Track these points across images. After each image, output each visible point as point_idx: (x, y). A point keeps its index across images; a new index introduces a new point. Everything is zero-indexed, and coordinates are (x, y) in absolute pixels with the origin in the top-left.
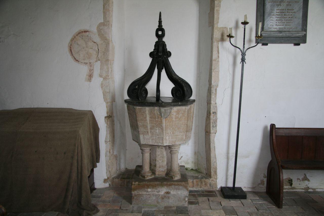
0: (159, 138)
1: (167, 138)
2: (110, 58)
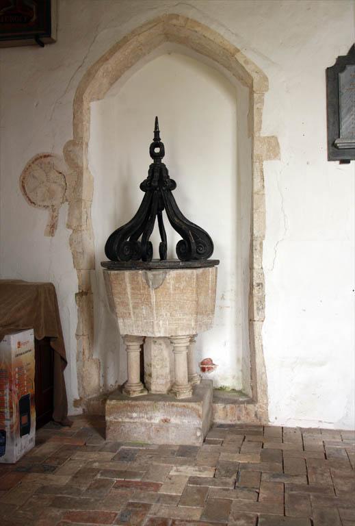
0: (147, 323)
1: (161, 323)
2: (85, 195)
